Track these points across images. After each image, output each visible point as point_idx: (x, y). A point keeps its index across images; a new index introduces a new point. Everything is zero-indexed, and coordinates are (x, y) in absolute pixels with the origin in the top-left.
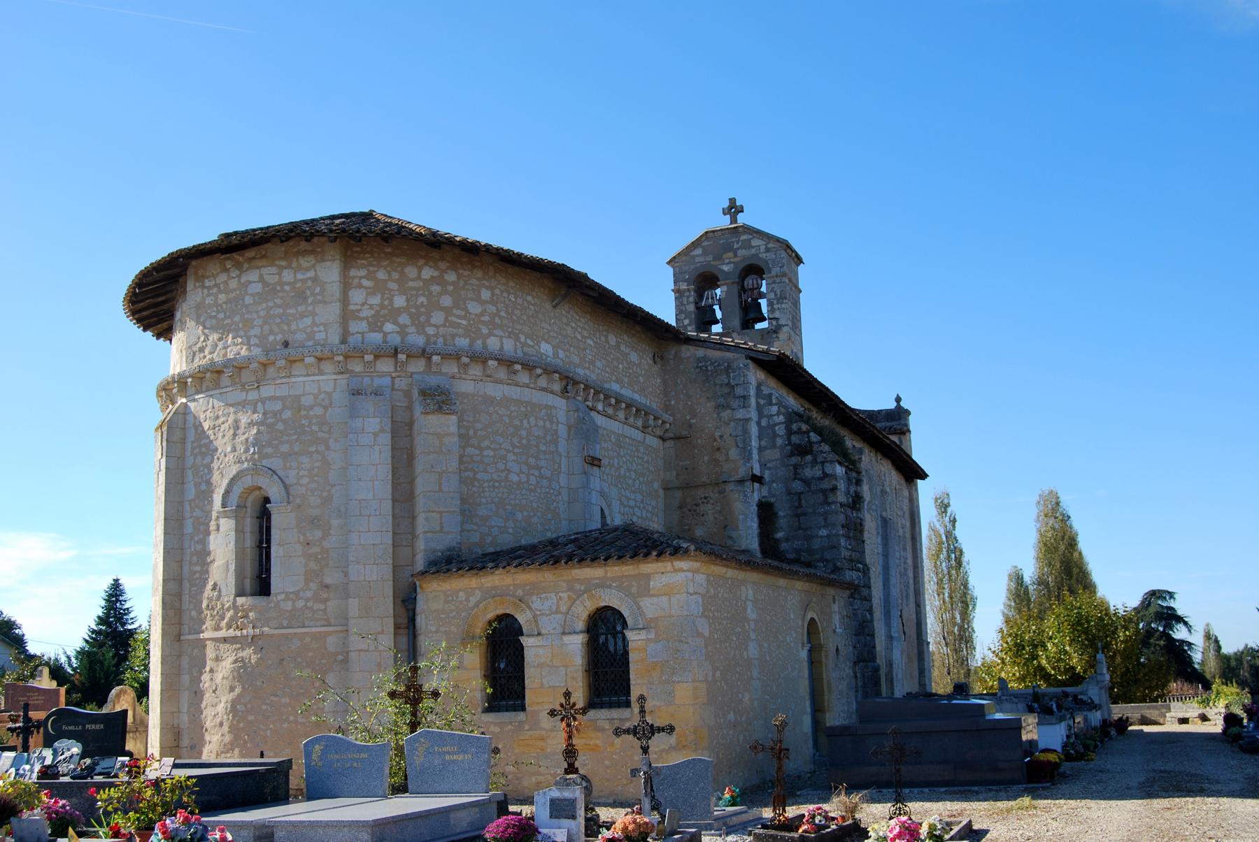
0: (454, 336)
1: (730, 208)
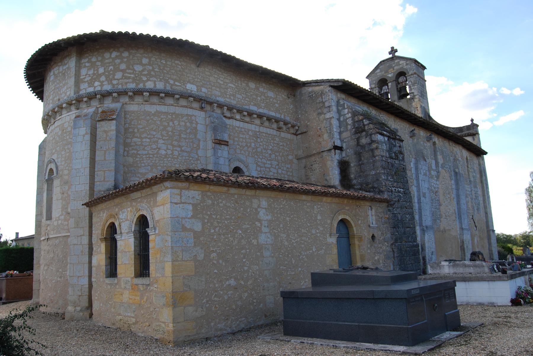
0: (126, 83)
1: (392, 51)
